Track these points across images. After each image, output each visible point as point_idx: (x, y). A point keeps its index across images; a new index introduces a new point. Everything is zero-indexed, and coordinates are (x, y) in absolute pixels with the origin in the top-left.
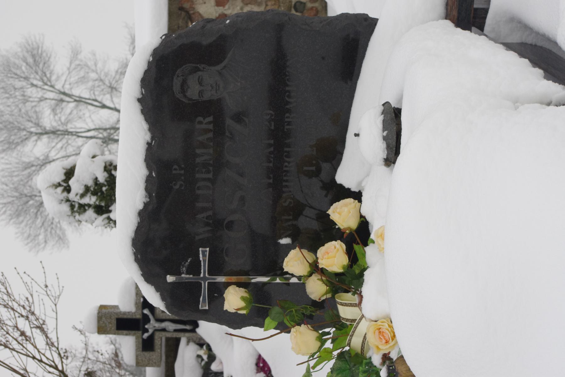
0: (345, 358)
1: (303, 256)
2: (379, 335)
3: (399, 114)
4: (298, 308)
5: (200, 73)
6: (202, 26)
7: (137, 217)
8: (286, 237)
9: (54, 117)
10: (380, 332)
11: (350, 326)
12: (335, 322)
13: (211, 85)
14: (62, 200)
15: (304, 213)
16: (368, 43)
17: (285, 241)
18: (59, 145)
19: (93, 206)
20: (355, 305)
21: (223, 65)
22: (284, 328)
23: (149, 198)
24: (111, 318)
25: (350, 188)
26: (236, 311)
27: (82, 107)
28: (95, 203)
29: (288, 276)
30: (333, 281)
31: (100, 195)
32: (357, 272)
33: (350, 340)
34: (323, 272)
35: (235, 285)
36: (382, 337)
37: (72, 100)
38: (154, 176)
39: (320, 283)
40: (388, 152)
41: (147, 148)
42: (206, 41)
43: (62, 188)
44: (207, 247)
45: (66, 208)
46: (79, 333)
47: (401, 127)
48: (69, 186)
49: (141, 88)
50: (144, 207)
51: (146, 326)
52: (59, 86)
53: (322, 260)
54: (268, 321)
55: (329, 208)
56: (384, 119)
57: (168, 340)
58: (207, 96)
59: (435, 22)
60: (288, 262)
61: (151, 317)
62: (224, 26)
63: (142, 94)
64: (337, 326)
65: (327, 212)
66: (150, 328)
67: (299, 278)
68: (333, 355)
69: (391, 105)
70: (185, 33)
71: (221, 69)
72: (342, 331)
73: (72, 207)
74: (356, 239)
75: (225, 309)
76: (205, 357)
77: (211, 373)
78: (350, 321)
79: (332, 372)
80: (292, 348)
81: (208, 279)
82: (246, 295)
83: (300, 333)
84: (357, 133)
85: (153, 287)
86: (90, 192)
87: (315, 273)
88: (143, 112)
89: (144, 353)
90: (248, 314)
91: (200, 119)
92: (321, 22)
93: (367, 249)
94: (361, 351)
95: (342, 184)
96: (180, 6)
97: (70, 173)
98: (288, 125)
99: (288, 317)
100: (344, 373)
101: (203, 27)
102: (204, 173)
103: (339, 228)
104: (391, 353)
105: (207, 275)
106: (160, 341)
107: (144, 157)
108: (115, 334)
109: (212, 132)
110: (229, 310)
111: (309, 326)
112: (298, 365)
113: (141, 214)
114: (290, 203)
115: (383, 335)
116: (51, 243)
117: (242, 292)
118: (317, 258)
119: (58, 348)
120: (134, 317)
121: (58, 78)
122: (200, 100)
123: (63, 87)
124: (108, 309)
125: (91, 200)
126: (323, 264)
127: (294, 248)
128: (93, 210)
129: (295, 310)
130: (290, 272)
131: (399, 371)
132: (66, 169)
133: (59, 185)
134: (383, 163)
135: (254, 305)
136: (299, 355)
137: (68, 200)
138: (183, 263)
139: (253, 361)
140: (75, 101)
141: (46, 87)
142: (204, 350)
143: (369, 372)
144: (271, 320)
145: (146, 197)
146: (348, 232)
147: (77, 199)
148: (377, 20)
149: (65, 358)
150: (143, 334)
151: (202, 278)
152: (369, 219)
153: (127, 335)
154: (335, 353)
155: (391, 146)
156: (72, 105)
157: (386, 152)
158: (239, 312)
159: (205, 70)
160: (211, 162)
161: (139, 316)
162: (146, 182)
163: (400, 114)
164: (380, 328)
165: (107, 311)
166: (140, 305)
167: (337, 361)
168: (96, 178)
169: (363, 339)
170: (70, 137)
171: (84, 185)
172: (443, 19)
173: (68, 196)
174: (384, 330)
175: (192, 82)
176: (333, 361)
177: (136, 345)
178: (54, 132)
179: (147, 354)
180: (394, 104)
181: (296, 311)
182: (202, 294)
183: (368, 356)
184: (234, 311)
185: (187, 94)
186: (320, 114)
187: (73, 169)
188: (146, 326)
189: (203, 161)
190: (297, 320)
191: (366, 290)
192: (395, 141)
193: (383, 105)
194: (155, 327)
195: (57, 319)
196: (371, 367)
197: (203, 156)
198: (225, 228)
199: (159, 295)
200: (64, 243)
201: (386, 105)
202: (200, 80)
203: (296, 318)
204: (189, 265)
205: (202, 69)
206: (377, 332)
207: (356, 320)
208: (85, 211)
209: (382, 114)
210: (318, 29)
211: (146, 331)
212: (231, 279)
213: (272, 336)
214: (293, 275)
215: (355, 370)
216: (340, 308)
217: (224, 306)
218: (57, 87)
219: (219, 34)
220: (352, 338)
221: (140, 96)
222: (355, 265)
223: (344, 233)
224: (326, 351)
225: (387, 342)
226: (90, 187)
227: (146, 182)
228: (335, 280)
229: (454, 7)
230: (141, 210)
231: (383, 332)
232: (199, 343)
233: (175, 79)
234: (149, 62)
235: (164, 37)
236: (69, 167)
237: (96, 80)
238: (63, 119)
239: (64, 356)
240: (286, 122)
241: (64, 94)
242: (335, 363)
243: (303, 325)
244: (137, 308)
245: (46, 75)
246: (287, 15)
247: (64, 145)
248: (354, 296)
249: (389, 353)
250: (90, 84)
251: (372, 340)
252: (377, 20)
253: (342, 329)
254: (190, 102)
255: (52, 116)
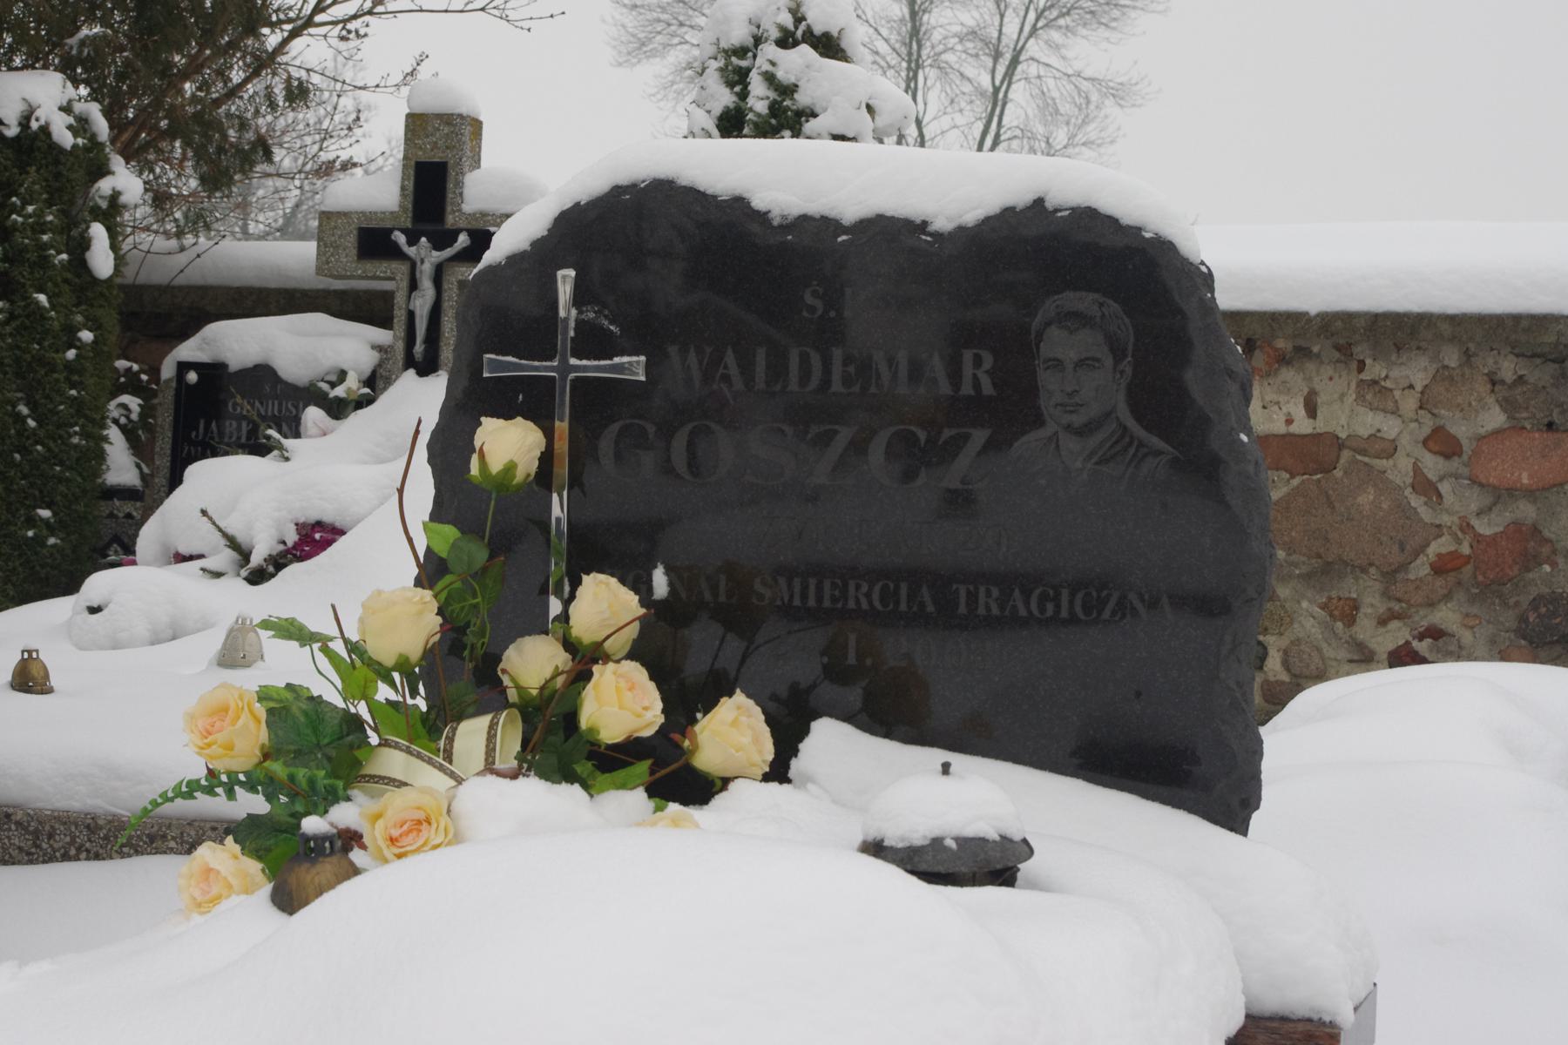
0: (348, 735)
1: (621, 625)
2: (412, 821)
3: (1001, 880)
4: (484, 611)
5: (1109, 361)
6: (1232, 372)
7: (729, 193)
8: (671, 584)
9: (955, 35)
10: (421, 823)
11: (433, 745)
12: (445, 710)
13: (1076, 391)
14: (758, 27)
15: (729, 636)
16: (1184, 810)
17: (660, 582)
18: (882, 47)
19: (742, 104)
20: (491, 759)
21: (1131, 423)
22: (431, 571)
23: (781, 226)
24: (447, 148)
25: (800, 755)
26: (477, 449)
27: (981, 107)
28: (751, 109)
29: (567, 588)
30: (553, 704)
31: (770, 123)
32: (579, 769)
33: (397, 746)
34: (581, 676)
35: (546, 447)
36: (405, 827)
37: (997, 83)
38: (840, 239)
39: (548, 673)
40: (900, 849)
41: (912, 222)
42: (1192, 378)
43: (790, 25)
44: (647, 377)
45: (739, 34)
46: (409, 70)
47: (966, 886)
48: (795, 44)
49: (1073, 209)
50: (758, 212)
51: (423, 239)
52: (1033, 48)
53: (615, 673)
54: (450, 532)
55: (749, 696)
56: (988, 841)
57: (388, 297)
58: (1048, 381)
59: (1240, 985)
60: (607, 584)
61: (448, 252)
62: (1232, 429)
63: (1056, 210)
64: (433, 716)
65: (738, 691)
66: (418, 250)
67: (565, 617)
68: (356, 702)
69: (1026, 860)
70: (1217, 324)
71: (1118, 418)
72: (419, 726)
73: (741, 52)
74: (663, 768)
75: (483, 419)
76: (339, 392)
77: (296, 407)
78: (448, 747)
79: (312, 698)
80: (380, 592)
81: (563, 378)
82: (520, 476)
83: (420, 613)
84: (952, 769)
85: (546, 233)
86: (779, 99)
87: (573, 660)
88: (1008, 212)
89: (355, 232)
90: (468, 482)
91: (988, 361)
92: (1239, 684)
93: (640, 795)
94: (366, 776)
95: (811, 735)
96: (1258, 343)
97: (829, 46)
98: (969, 592)
99: (458, 585)
100: (308, 731)
101: (1231, 374)
102: (844, 371)
103: (694, 721)
104: (362, 852)
105: (573, 375)
106: (383, 277)
107: (889, 214)
108: (405, 158)
109: (952, 393)
110: (479, 431)
111: (438, 636)
112: (333, 607)
113: (739, 203)
114: (761, 597)
115: (410, 831)
116: (630, 20)
117: (527, 465)
118: (618, 661)
119: (370, 13)
120: (449, 209)
121: (1056, 47)
122: (1037, 362)
123: (1032, 59)
124: (472, 140)
125: (759, 98)
126: (601, 675)
127: (643, 603)
128: (732, 106)
129: (478, 603)
130: (580, 591)
131: (319, 867)
132: (838, 38)
133: (799, 19)
134: (870, 839)
135: (494, 496)
136: (360, 611)
137: (758, 40)
138: (606, 312)
139: (329, 515)
140: (996, 90)
141: (1032, 16)
142: (359, 389)
143: (310, 794)
144: (451, 541)
145: (784, 217)
146: (687, 743)
147: (762, 63)
148: (1244, 833)
149: (344, 33)
150: (403, 231)
151: (567, 361)
152: (719, 801)
153: (403, 188)
154: (362, 710)
155: (916, 859)
156: (985, 81)
157: (900, 845)
158: (475, 460)
159: (1118, 376)
160: (873, 390)
161: (450, 220)
162: (822, 217)
163: (1001, 885)
164: (430, 824)
165: (466, 138)
166: (480, 225)
167: (341, 713)
168: (815, 115)
169: (399, 781)
170: (903, 74)
171: (799, 84)
172: (1247, 1008)
173: (769, 42)
174: (425, 834)
175: (1087, 342)
176: (341, 704)
177: (376, 213)
178: (915, 34)
179: (351, 241)
180: (1025, 868)
181: (475, 606)
182: (523, 362)
183: (354, 793)
184: (477, 444)
185: (1053, 327)
186: (997, 679)
187: (837, 53)
188: (423, 239)
189: (877, 369)
190: (450, 608)
191: (533, 788)
192: (930, 870)
193: (1025, 841)
194: (422, 261)
195: (446, 11)
196: (325, 799)
197: (890, 367)
198: (694, 428)
199: (522, 250)
200: (629, 53)
201: (1025, 849)
202: (1090, 362)
203: (457, 607)
204: (602, 328)
205: (1121, 367)
206: (421, 815)
207: (451, 762)
208: (730, 85)
209: (1001, 836)
210: (1222, 675)
211: (413, 241)
212: (560, 439)
213: (410, 540)
214: (567, 603)
215: (317, 758)
216: (483, 721)
217: (492, 416)
218: (1032, 41)
219: (1211, 415)
220: (402, 750)
221: (1049, 205)
222: (593, 765)
223: (684, 735)
224: (368, 684)
225: (393, 840)
226: (792, 99)
227: (822, 217)
228: (554, 710)
229: (1277, 1037)
230: (749, 203)
231: (420, 831)
232: (378, 375)
233: (1096, 296)
234: (1140, 229)
235: (1204, 269)
236: (844, 45)
237: (1048, 142)
238: (949, 57)
239: (349, 32)
240: (977, 589)
241: (1015, 62)
242: (336, 707)
243: (439, 620)
244: (473, 216)
245: (1062, 15)
246: (1260, 594)
247: (884, 58)
248: (515, 758)
249: (363, 847)
250: (1040, 129)
251: (397, 803)
252: (1244, 833)
253: (424, 727)
254: (1033, 336)
255: (956, 29)
